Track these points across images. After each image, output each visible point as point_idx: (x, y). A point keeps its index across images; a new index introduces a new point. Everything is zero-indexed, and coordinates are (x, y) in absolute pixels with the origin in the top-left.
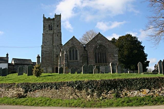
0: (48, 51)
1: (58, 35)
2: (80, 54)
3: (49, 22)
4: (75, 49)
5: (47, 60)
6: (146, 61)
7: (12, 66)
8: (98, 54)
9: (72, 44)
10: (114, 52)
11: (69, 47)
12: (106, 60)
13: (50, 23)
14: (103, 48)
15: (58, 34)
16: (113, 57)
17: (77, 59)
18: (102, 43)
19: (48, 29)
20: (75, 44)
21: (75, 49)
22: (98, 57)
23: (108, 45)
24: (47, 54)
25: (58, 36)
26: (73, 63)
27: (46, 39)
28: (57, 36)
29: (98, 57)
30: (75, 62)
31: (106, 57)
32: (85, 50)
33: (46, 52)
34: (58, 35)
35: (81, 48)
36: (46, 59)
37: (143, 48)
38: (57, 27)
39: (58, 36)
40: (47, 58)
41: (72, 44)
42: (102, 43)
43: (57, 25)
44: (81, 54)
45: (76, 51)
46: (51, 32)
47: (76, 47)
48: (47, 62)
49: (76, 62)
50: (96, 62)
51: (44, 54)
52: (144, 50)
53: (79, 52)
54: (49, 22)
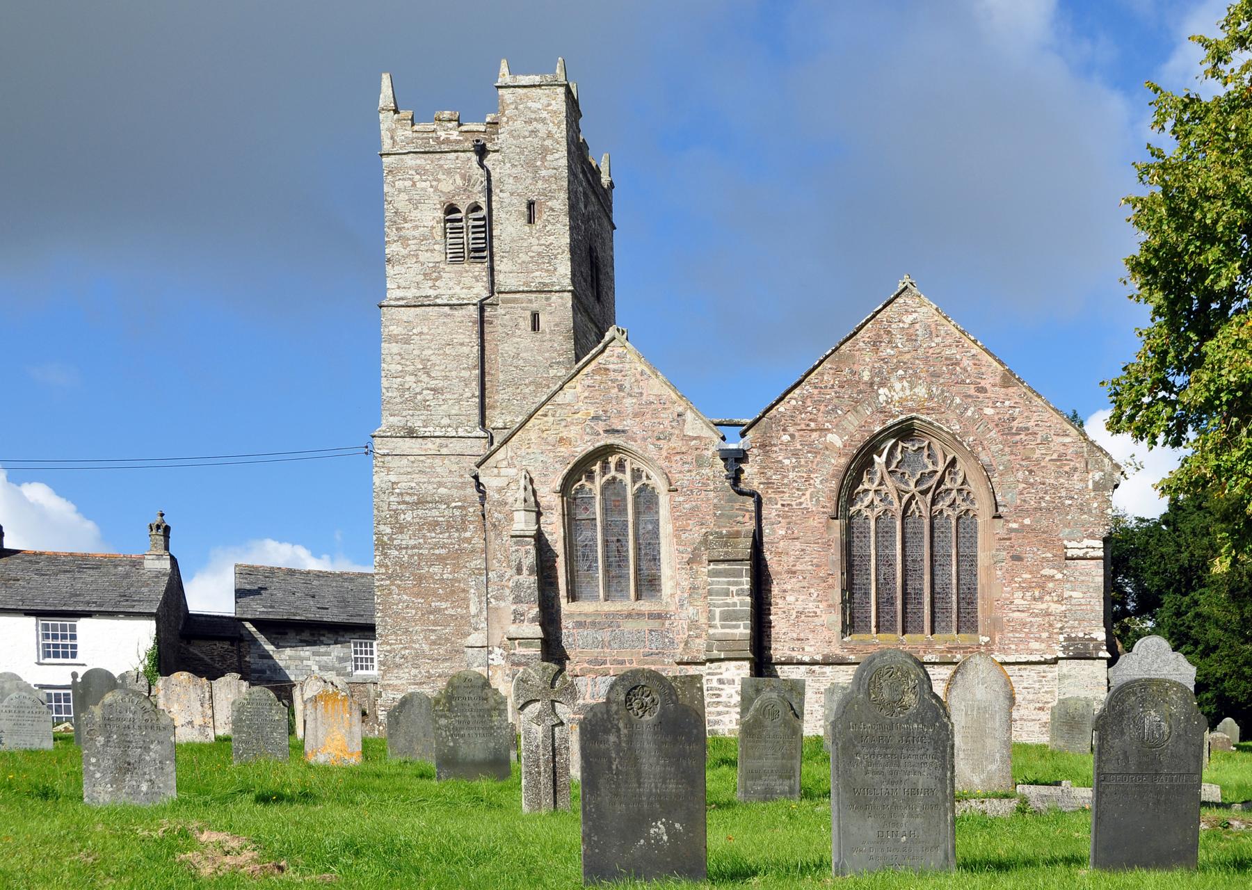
0: (446, 501)
1: (535, 316)
4: (627, 477)
5: (435, 594)
6: (665, 838)
7: (226, 645)
8: (884, 533)
9: (600, 426)
10: (1062, 509)
11: (563, 450)
12: (968, 599)
13: (459, 182)
14: (941, 467)
15: (535, 306)
20: (627, 424)
21: (637, 475)
22: (885, 561)
23: (1006, 427)
25: (535, 327)
26: (606, 635)
27: (425, 361)
28: (526, 324)
29: (885, 561)
30: (629, 626)
31: (968, 561)
32: (741, 493)
33: (421, 502)
34: (535, 316)
36: (420, 578)
38: (531, 220)
39: (535, 327)
41: (600, 426)
43: (531, 205)
44: (696, 534)
45: (646, 499)
47: (648, 461)
48: (438, 610)
49: (645, 625)
50: (850, 625)
51: (401, 528)
53: (674, 508)
54: (449, 172)
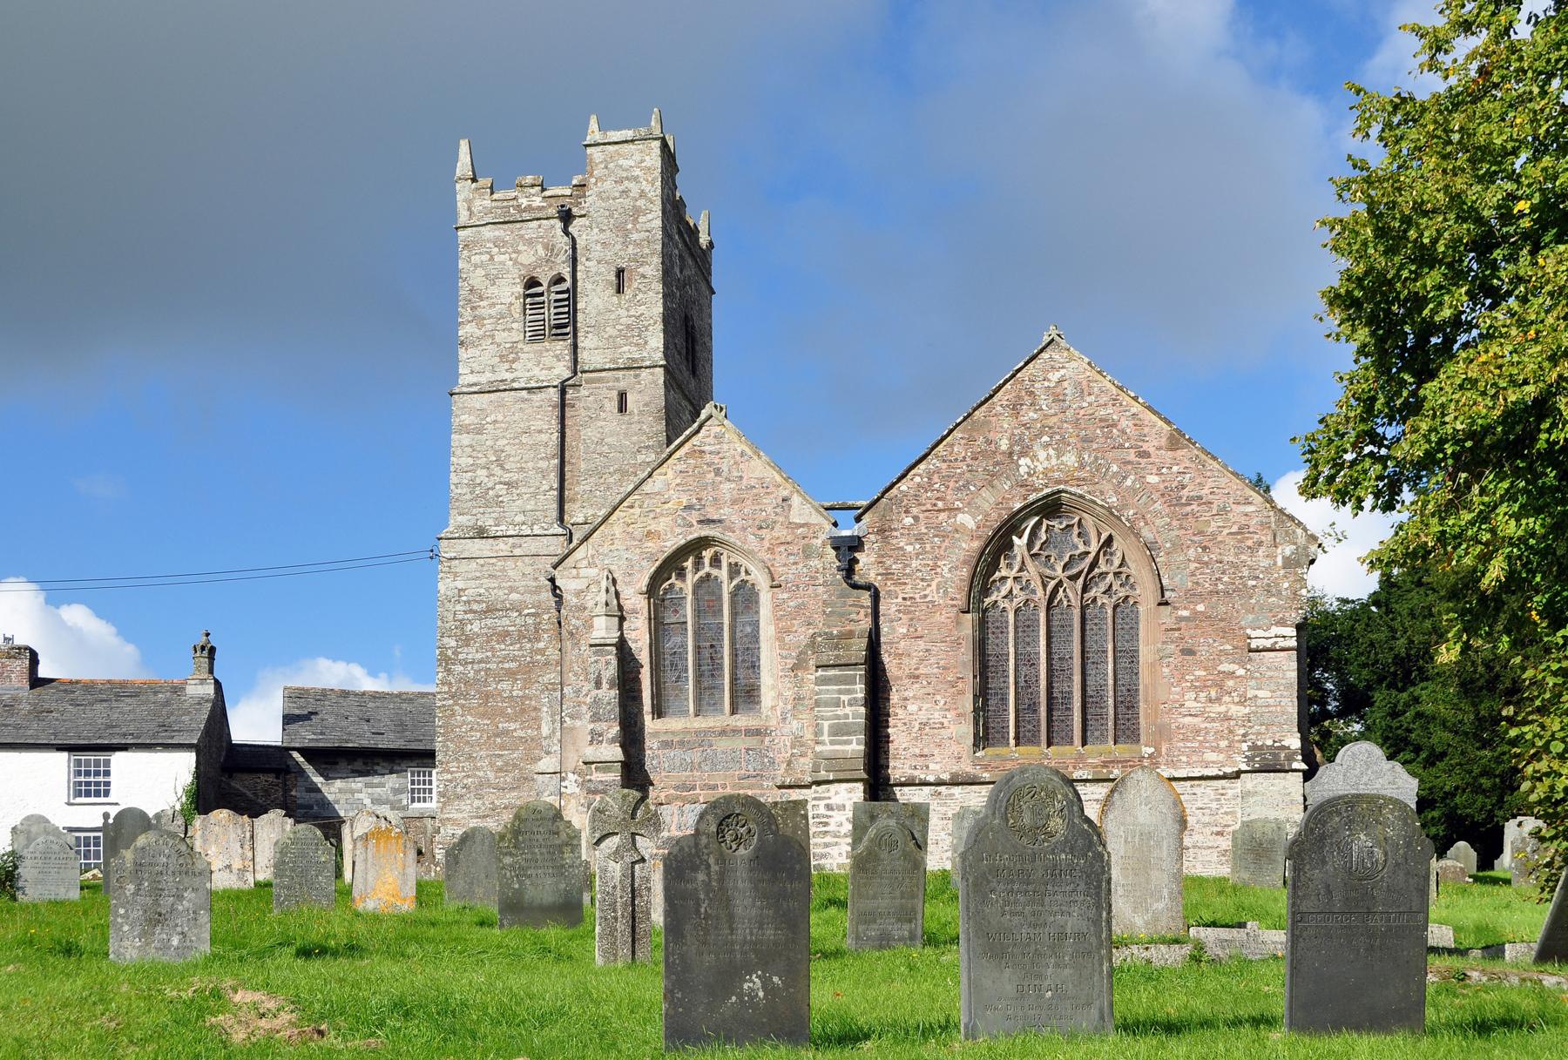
1: (622, 396)
2: (782, 633)
3: (530, 242)
4: (723, 574)
5: (503, 713)
7: (271, 778)
9: (694, 517)
10: (1242, 591)
11: (651, 546)
12: (1127, 703)
15: (622, 385)
16: (1225, 667)
17: (745, 696)
18: (1080, 481)
19: (515, 332)
20: (725, 512)
21: (734, 570)
22: (1026, 660)
23: (1173, 497)
24: (505, 635)
25: (622, 407)
26: (696, 756)
29: (1026, 660)
30: (722, 744)
31: (1127, 657)
32: (855, 586)
33: (490, 610)
34: (622, 396)
35: (807, 553)
37: (119, 633)
38: (619, 290)
39: (622, 407)
40: (505, 685)
41: (694, 517)
42: (1080, 481)
43: (620, 273)
44: (802, 635)
45: (745, 597)
46: (551, 363)
48: (506, 732)
49: (741, 743)
50: (983, 738)
52: (1365, 597)
53: (777, 606)
54: (530, 242)
